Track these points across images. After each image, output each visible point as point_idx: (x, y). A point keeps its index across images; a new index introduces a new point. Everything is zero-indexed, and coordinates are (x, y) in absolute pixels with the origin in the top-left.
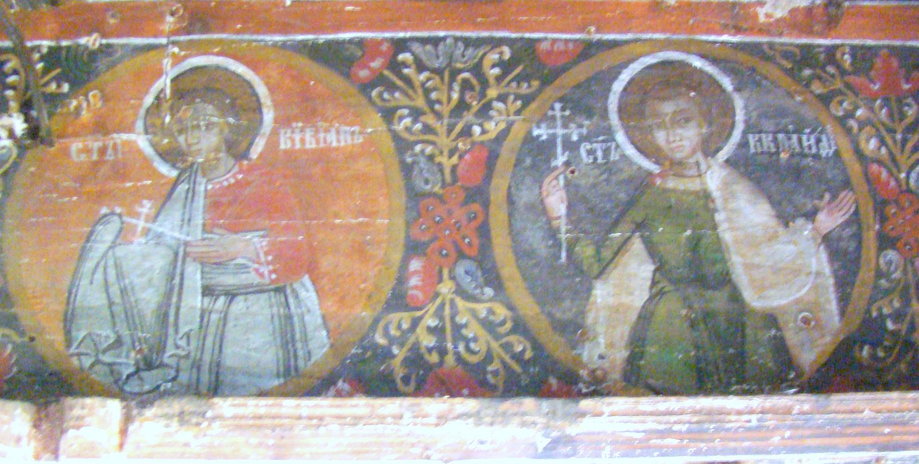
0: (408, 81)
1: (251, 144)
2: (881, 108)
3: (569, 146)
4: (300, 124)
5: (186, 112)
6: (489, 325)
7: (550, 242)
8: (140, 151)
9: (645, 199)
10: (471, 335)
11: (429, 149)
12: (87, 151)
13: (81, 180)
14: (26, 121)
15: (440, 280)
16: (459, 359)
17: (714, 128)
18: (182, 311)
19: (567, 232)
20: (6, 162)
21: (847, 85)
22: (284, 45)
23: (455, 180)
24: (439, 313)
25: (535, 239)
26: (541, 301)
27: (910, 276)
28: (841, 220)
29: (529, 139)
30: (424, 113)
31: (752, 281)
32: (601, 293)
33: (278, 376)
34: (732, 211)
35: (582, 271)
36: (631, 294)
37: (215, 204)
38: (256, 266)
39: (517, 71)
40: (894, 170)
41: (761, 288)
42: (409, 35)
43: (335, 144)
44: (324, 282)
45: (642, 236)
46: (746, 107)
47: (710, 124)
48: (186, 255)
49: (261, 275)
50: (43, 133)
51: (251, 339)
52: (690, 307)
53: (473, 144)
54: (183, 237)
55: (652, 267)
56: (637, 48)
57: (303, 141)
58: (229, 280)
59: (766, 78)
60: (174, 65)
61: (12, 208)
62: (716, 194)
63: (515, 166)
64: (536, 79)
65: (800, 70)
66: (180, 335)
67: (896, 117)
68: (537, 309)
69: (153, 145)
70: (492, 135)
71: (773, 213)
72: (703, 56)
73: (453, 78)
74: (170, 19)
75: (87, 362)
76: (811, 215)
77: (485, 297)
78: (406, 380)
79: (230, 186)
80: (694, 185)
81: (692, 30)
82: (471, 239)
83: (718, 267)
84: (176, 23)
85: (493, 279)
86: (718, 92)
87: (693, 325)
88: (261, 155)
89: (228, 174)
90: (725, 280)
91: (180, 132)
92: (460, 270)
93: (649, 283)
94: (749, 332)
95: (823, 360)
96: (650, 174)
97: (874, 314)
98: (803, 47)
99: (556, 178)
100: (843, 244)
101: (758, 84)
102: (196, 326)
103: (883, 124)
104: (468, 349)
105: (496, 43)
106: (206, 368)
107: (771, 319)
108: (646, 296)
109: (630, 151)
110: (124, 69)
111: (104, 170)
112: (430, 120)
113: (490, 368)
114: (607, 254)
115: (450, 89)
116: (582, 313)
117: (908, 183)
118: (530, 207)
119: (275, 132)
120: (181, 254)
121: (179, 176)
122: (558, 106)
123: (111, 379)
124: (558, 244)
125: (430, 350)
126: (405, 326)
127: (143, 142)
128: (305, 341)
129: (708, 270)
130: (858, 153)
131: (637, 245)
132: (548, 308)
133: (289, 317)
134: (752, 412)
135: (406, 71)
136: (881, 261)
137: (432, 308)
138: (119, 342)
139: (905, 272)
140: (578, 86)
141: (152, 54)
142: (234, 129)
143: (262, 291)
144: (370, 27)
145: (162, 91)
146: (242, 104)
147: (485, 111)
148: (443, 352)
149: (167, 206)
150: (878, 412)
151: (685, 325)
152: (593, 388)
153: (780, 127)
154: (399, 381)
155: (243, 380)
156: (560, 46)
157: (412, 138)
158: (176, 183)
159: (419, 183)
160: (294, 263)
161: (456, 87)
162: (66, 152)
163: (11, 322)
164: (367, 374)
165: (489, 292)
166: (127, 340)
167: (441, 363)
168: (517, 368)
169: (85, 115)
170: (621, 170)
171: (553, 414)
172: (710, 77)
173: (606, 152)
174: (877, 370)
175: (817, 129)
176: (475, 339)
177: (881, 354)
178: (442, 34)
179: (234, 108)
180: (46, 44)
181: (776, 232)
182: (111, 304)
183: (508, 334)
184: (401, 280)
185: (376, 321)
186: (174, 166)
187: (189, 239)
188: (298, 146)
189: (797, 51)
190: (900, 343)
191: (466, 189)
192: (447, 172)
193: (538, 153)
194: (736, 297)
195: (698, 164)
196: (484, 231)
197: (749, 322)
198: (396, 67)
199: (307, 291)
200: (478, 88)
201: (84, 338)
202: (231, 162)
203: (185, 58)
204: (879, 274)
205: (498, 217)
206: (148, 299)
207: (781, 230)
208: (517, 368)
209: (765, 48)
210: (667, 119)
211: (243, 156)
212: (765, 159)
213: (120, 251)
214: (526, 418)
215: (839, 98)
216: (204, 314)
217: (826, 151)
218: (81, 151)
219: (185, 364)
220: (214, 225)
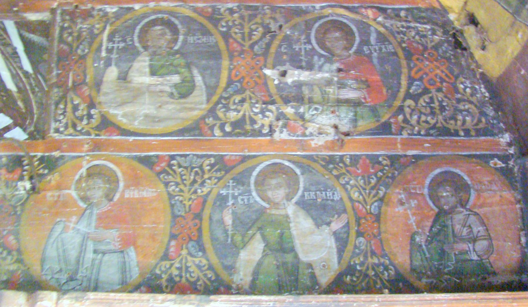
0: (174, 171)
1: (114, 195)
2: (361, 180)
3: (235, 197)
4: (133, 188)
5: (91, 182)
7: (225, 235)
8: (72, 197)
10: (192, 270)
15: (182, 249)
16: (187, 279)
17: (291, 190)
18: (85, 259)
19: (232, 231)
21: (348, 171)
22: (128, 157)
25: (219, 233)
26: (220, 258)
27: (369, 248)
28: (341, 226)
29: (219, 195)
30: (180, 184)
32: (243, 255)
33: (119, 285)
34: (297, 222)
35: (236, 246)
37: (100, 218)
38: (113, 242)
39: (216, 168)
40: (365, 205)
43: (145, 196)
46: (304, 181)
47: (289, 188)
48: (88, 238)
49: (115, 246)
50: (37, 190)
51: (110, 271)
52: (277, 261)
53: (198, 196)
55: (264, 245)
56: (264, 158)
57: (134, 195)
58: (103, 248)
60: (88, 163)
62: (291, 216)
63: (213, 205)
65: (328, 165)
67: (367, 183)
69: (79, 195)
70: (205, 193)
71: (313, 223)
72: (289, 161)
74: (86, 146)
75: (49, 277)
76: (328, 224)
78: (167, 287)
79: (105, 211)
80: (282, 212)
81: (285, 150)
82: (195, 233)
84: (88, 147)
87: (278, 267)
88: (118, 200)
89: (105, 206)
90: (292, 250)
91: (89, 190)
93: (262, 251)
94: (300, 271)
96: (265, 208)
98: (330, 156)
99: (228, 210)
100: (341, 235)
101: (311, 172)
102: (90, 265)
103: (361, 186)
104: (191, 275)
105: (209, 156)
107: (310, 266)
108: (260, 256)
109: (258, 199)
110: (68, 166)
112: (182, 187)
113: (199, 283)
114: (246, 239)
115: (190, 175)
116: (235, 262)
117: (370, 210)
118: (218, 221)
119: (123, 191)
120: (86, 238)
121: (87, 207)
123: (57, 284)
124: (227, 236)
125: (176, 276)
126: (168, 266)
127: (74, 193)
130: (351, 199)
131: (258, 236)
132: (222, 261)
133: (124, 263)
134: (271, 301)
135: (174, 168)
136: (357, 242)
137: (178, 260)
138: (61, 271)
139: (366, 246)
140: (239, 174)
141: (80, 159)
142: (109, 189)
143: (116, 252)
144: (161, 150)
145: (82, 174)
146: (111, 179)
147: (203, 184)
148: (181, 277)
149: (82, 218)
150: (318, 302)
151: (275, 267)
152: (237, 291)
154: (164, 287)
155: (107, 286)
158: (86, 210)
160: (128, 241)
161: (193, 174)
162: (45, 196)
164: (151, 285)
165: (200, 254)
167: (180, 281)
169: (53, 183)
171: (200, 301)
172: (291, 169)
173: (248, 199)
174: (354, 286)
176: (193, 272)
177: (355, 279)
178: (188, 153)
179: (109, 181)
180: (40, 154)
182: (59, 256)
183: (206, 270)
184: (167, 249)
185: (157, 264)
187: (89, 231)
188: (132, 197)
189: (328, 158)
191: (195, 214)
192: (187, 207)
193: (222, 200)
194: (296, 257)
195: (284, 204)
196: (200, 230)
197: (301, 266)
198: (170, 166)
199: (132, 252)
200: (201, 174)
201: (48, 269)
202: (107, 202)
203: (91, 161)
204: (355, 247)
205: (205, 225)
206: (73, 254)
207: (316, 230)
208: (209, 283)
211: (111, 200)
213: (64, 235)
214: (192, 302)
215: (344, 176)
216: (93, 260)
217: (336, 198)
218: (51, 196)
219: (85, 279)
220: (99, 227)
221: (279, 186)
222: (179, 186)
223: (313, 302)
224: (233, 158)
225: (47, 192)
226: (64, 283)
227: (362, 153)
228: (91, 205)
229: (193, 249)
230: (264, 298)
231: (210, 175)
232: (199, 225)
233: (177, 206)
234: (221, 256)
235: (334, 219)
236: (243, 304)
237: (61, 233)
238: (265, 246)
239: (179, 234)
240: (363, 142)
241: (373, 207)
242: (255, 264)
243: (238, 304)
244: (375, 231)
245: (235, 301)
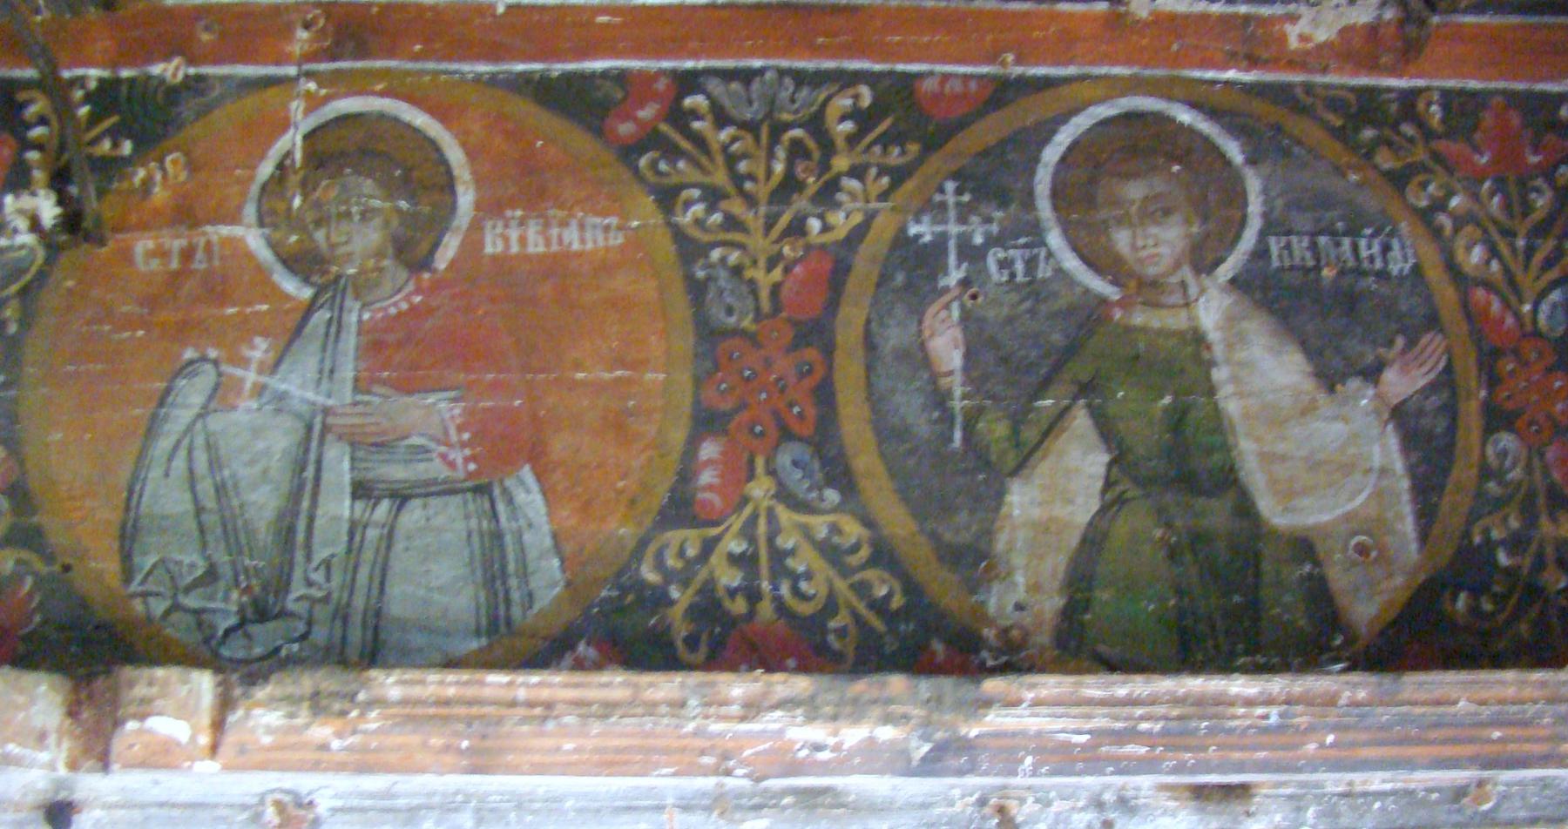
0: (700, 141)
1: (436, 245)
2: (1492, 194)
3: (971, 254)
4: (519, 213)
5: (327, 190)
6: (831, 552)
7: (936, 414)
8: (250, 255)
10: (801, 569)
11: (734, 257)
12: (162, 253)
13: (151, 302)
15: (751, 476)
16: (781, 607)
17: (1211, 226)
18: (319, 523)
19: (964, 397)
20: (26, 271)
21: (1435, 156)
22: (493, 80)
23: (777, 307)
24: (748, 532)
25: (910, 407)
27: (1538, 475)
28: (1422, 383)
29: (902, 241)
30: (726, 196)
31: (1273, 482)
32: (1021, 500)
33: (478, 633)
34: (1240, 364)
35: (988, 463)
36: (1071, 502)
37: (375, 345)
38: (443, 449)
40: (1513, 300)
41: (1287, 494)
44: (556, 477)
45: (1089, 406)
46: (1265, 191)
47: (1205, 219)
48: (325, 429)
49: (452, 465)
50: (87, 224)
52: (1169, 525)
53: (808, 248)
55: (1106, 458)
56: (1084, 91)
57: (523, 240)
58: (397, 473)
60: (309, 111)
62: (1214, 336)
63: (878, 285)
65: (1357, 130)
66: (315, 564)
67: (1517, 209)
69: (273, 245)
70: (840, 234)
71: (1309, 369)
72: (1194, 105)
74: (303, 35)
75: (159, 607)
76: (1372, 374)
78: (692, 642)
80: (1176, 321)
81: (1177, 61)
82: (802, 408)
85: (840, 474)
87: (1173, 554)
88: (453, 264)
89: (397, 295)
90: (1228, 480)
91: (318, 223)
92: (784, 459)
93: (1100, 484)
94: (1267, 567)
95: (1391, 615)
96: (1103, 301)
97: (1477, 539)
99: (947, 307)
100: (1425, 422)
101: (1286, 153)
102: (341, 549)
103: (1495, 222)
104: (796, 592)
105: (848, 80)
106: (357, 619)
107: (1303, 546)
108: (1095, 505)
109: (1071, 263)
111: (189, 286)
112: (737, 207)
113: (833, 624)
114: (1030, 434)
115: (771, 155)
116: (988, 533)
117: (1535, 322)
118: (902, 355)
119: (476, 226)
120: (317, 428)
122: (950, 186)
123: (197, 637)
124: (948, 418)
125: (732, 593)
126: (691, 552)
127: (254, 240)
128: (524, 575)
130: (1453, 269)
131: (1081, 420)
132: (930, 525)
133: (497, 536)
134: (1270, 702)
135: (696, 125)
136: (1490, 451)
137: (737, 522)
138: (211, 575)
139: (1529, 469)
140: (985, 153)
141: (272, 92)
144: (638, 51)
146: (421, 177)
147: (828, 194)
148: (753, 596)
150: (1482, 703)
151: (1161, 555)
152: (1004, 659)
154: (679, 644)
155: (418, 640)
157: (706, 238)
158: (310, 308)
159: (717, 314)
160: (505, 445)
161: (781, 153)
162: (126, 256)
165: (832, 496)
166: (226, 571)
167: (751, 614)
168: (878, 624)
169: (159, 194)
170: (1055, 295)
171: (936, 702)
172: (1206, 139)
173: (1031, 264)
175: (1384, 229)
176: (808, 576)
177: (1488, 606)
178: (757, 63)
179: (408, 185)
180: (94, 73)
181: (1314, 400)
182: (199, 510)
183: (863, 567)
185: (643, 543)
186: (307, 281)
187: (330, 402)
188: (515, 249)
189: (1352, 97)
191: (795, 324)
192: (764, 295)
194: (1245, 508)
195: (1183, 285)
196: (825, 394)
197: (1268, 550)
198: (680, 117)
200: (816, 155)
201: (154, 566)
202: (403, 274)
203: (327, 99)
204: (1486, 472)
207: (1322, 398)
208: (878, 624)
209: (1299, 92)
211: (425, 264)
212: (1296, 279)
213: (216, 422)
215: (1421, 178)
216: (355, 528)
217: (1398, 265)
218: (151, 254)
219: (322, 613)
221: (1156, 211)
222: (724, 205)
223: (1461, 704)
224: (957, 86)
225: (136, 234)
226: (227, 632)
227: (1493, 85)
228: (331, 290)
229: (798, 474)
230: (1239, 686)
231: (861, 160)
232: (820, 372)
233: (721, 292)
234: (926, 505)
235: (1392, 354)
236: (1142, 718)
237: (203, 414)
238: (1110, 465)
239: (736, 411)
240: (1492, 37)
241: (1545, 307)
242: (1074, 540)
243: (1116, 718)
244: (1559, 407)
245: (1103, 703)
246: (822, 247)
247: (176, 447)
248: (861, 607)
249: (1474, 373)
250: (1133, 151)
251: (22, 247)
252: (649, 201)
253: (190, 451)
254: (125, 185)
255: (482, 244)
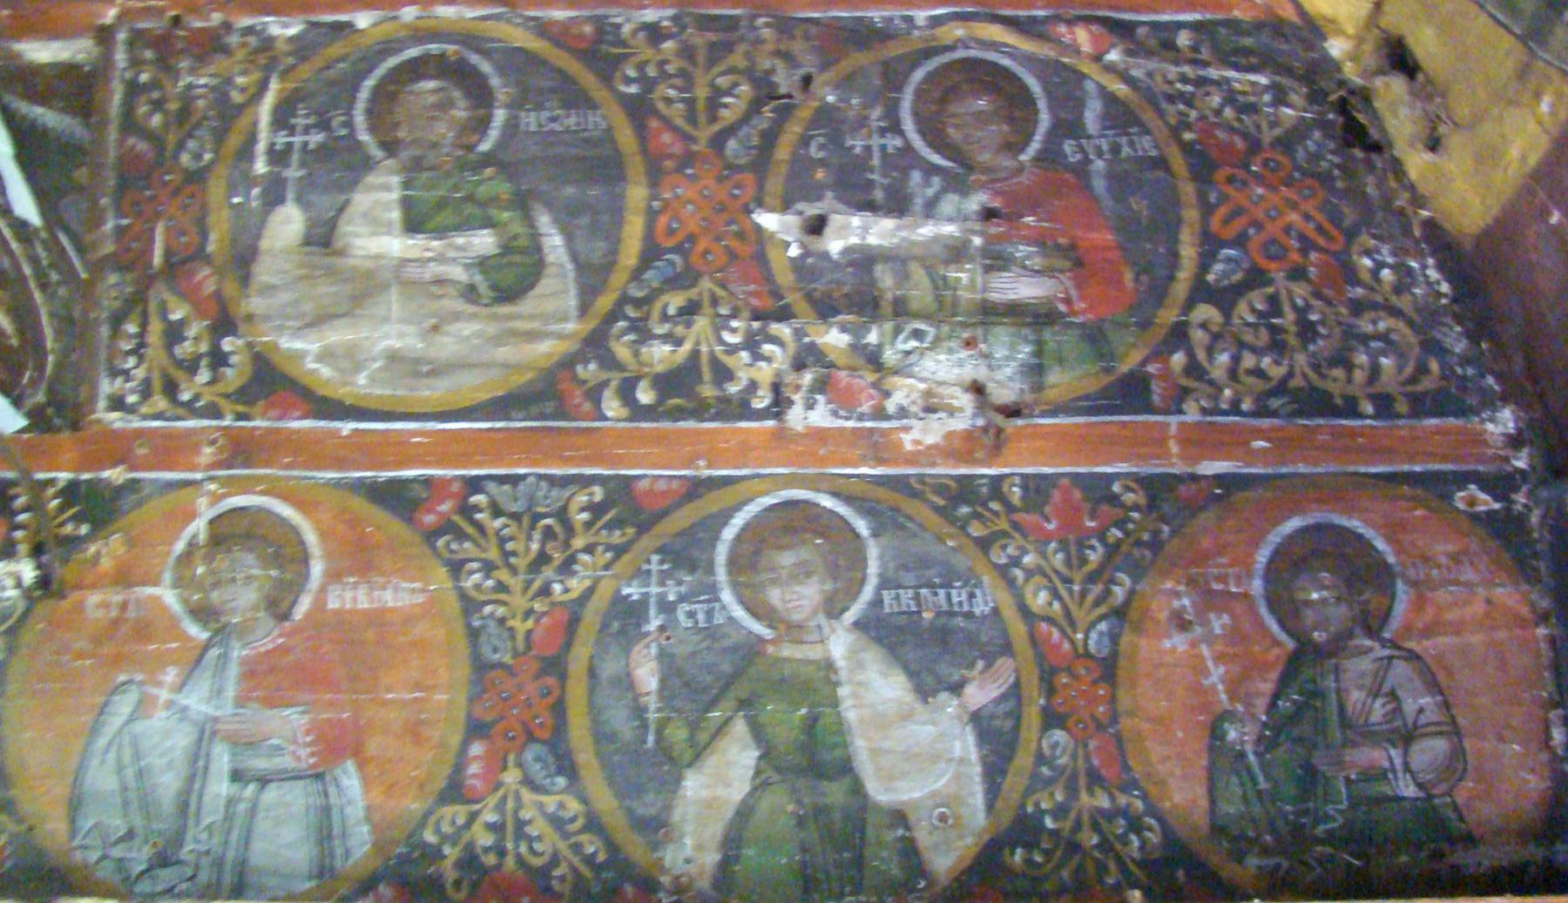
0: (480, 527)
1: (294, 603)
3: (667, 608)
4: (352, 580)
5: (222, 562)
6: (557, 823)
7: (636, 723)
8: (165, 609)
9: (752, 671)
10: (535, 833)
11: (501, 611)
12: (106, 605)
13: (97, 641)
14: (39, 567)
15: (505, 768)
16: (520, 860)
17: (839, 585)
18: (207, 799)
19: (659, 710)
20: (10, 616)
21: (1016, 526)
22: (338, 484)
23: (529, 647)
24: (500, 807)
25: (618, 718)
26: (621, 795)
27: (1081, 762)
28: (995, 694)
29: (619, 600)
31: (879, 769)
32: (694, 785)
33: (310, 878)
34: (860, 684)
36: (729, 786)
37: (252, 672)
39: (608, 517)
40: (1069, 630)
41: (889, 778)
42: (482, 472)
43: (391, 604)
44: (372, 769)
45: (745, 716)
46: (881, 557)
48: (214, 733)
49: (299, 759)
50: (55, 586)
52: (799, 802)
53: (553, 604)
54: (211, 711)
55: (757, 754)
57: (355, 600)
58: (260, 764)
59: (911, 519)
60: (212, 504)
61: (17, 668)
63: (600, 631)
64: (633, 525)
65: (955, 508)
66: (202, 826)
67: (1075, 561)
68: (615, 804)
69: (185, 601)
70: (574, 595)
71: (909, 686)
72: (835, 494)
73: (533, 527)
74: (208, 450)
75: (94, 856)
76: (957, 688)
77: (556, 788)
80: (814, 653)
81: (823, 461)
82: (544, 718)
83: (838, 753)
85: (567, 766)
86: (850, 536)
87: (801, 822)
90: (846, 768)
92: (529, 756)
93: (751, 773)
94: (870, 833)
95: (967, 863)
96: (761, 640)
97: (1030, 809)
98: (959, 479)
99: (647, 646)
100: (997, 723)
101: (902, 527)
102: (219, 816)
103: (1057, 572)
104: (531, 849)
106: (228, 867)
107: (899, 817)
108: (747, 788)
109: (739, 613)
110: (152, 510)
111: (124, 628)
112: (503, 575)
113: (557, 873)
114: (703, 737)
115: (529, 538)
116: (668, 808)
119: (323, 589)
120: (207, 733)
121: (210, 639)
122: (655, 558)
123: (118, 877)
124: (644, 726)
125: (487, 850)
126: (461, 821)
127: (169, 597)
128: (344, 835)
129: (826, 756)
130: (1025, 611)
131: (740, 727)
132: (628, 803)
133: (326, 810)
135: (478, 516)
136: (1045, 744)
137: (492, 801)
138: (130, 835)
139: (1074, 757)
140: (680, 534)
142: (280, 584)
143: (301, 778)
144: (439, 464)
145: (195, 536)
146: (285, 552)
147: (567, 567)
148: (502, 852)
149: (196, 673)
151: (793, 822)
153: (923, 581)
154: (448, 886)
156: (662, 486)
157: (482, 598)
158: (206, 647)
159: (486, 651)
160: (337, 744)
161: (537, 535)
162: (80, 607)
163: (7, 806)
165: (561, 781)
166: (140, 831)
167: (499, 867)
168: (586, 872)
169: (106, 564)
170: (724, 636)
172: (841, 518)
173: (709, 614)
174: (1035, 879)
175: (970, 580)
176: (539, 838)
177: (1038, 858)
178: (522, 471)
179: (278, 560)
180: (64, 476)
181: (912, 710)
182: (125, 789)
185: (427, 815)
186: (205, 626)
187: (218, 713)
188: (348, 606)
189: (953, 484)
190: (1062, 847)
191: (543, 659)
192: (520, 638)
193: (629, 615)
194: (858, 789)
195: (819, 627)
196: (559, 709)
197: (872, 819)
198: (467, 511)
199: (350, 779)
200: (561, 536)
202: (271, 622)
203: (224, 496)
204: (1040, 758)
205: (577, 691)
206: (168, 784)
207: (919, 706)
208: (586, 872)
209: (912, 481)
210: (784, 573)
211: (285, 616)
212: (903, 620)
213: (138, 727)
215: (1003, 542)
216: (231, 802)
218: (98, 606)
219: (205, 861)
221: (802, 572)
222: (496, 574)
228: (222, 633)
229: (538, 766)
231: (592, 540)
232: (556, 693)
234: (626, 790)
235: (975, 673)
237: (131, 720)
238: (761, 758)
239: (495, 722)
240: (1062, 434)
241: (1094, 636)
242: (729, 813)
244: (1101, 709)
246: (561, 603)
247: (110, 744)
248: (576, 861)
249: (1035, 681)
250: (790, 530)
251: (8, 599)
252: (442, 572)
253: (120, 747)
254: (81, 556)
255: (325, 604)
